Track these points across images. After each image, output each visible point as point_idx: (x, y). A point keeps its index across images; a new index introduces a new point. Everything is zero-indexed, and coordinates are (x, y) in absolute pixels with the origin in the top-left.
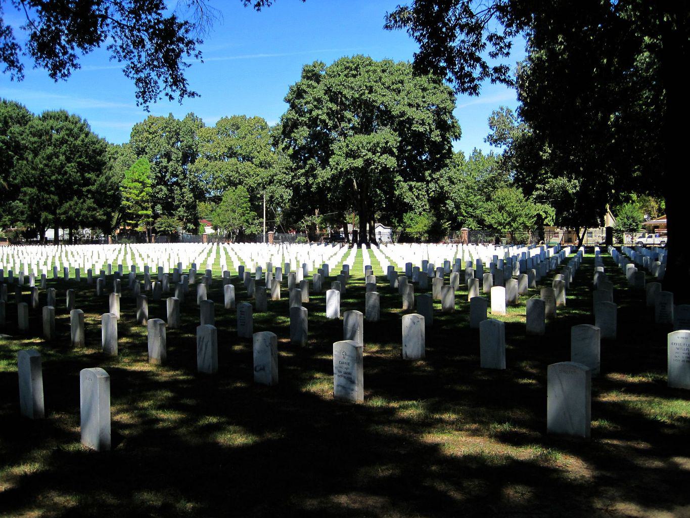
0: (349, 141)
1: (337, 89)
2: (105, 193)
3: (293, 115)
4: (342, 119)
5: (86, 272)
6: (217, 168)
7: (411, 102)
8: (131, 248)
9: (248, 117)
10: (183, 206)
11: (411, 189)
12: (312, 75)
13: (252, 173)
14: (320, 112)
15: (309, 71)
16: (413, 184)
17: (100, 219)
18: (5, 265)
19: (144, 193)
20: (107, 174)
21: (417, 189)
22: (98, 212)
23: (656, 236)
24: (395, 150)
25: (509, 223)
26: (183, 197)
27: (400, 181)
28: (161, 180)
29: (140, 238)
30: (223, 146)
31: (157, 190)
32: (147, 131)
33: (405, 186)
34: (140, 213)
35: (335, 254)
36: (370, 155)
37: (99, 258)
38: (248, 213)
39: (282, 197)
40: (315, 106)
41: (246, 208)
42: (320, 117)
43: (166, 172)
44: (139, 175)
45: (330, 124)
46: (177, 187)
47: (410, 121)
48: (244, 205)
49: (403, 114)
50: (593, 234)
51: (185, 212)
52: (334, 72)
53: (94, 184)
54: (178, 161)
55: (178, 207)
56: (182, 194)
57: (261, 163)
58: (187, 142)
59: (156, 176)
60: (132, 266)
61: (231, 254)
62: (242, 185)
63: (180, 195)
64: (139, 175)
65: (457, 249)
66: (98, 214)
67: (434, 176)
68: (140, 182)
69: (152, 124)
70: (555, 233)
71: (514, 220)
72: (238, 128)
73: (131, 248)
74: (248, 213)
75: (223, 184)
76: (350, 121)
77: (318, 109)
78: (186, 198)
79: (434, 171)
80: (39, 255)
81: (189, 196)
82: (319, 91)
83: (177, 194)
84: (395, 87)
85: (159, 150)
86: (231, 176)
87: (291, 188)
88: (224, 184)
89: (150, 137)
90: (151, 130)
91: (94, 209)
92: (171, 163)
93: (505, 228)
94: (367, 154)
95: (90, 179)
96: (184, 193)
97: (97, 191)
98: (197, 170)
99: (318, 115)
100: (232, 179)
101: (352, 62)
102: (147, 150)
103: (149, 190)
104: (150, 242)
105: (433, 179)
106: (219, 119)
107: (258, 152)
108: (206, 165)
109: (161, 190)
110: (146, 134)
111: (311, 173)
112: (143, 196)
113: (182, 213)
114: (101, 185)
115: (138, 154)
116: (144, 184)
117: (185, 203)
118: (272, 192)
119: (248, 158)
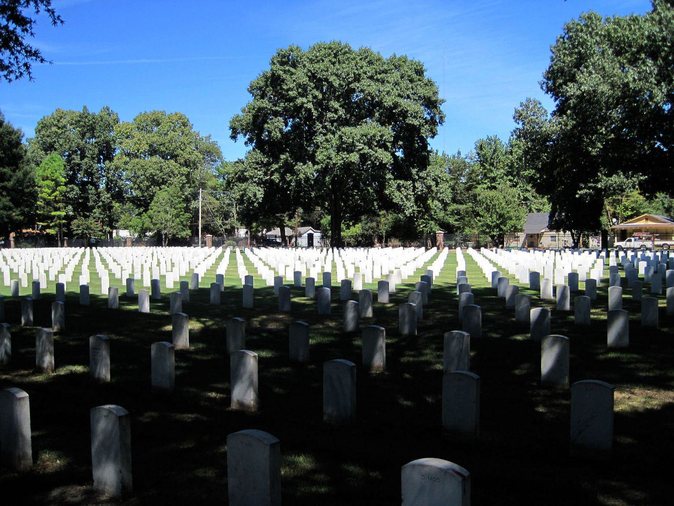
0: (342, 133)
1: (323, 75)
2: (22, 191)
3: (266, 104)
4: (328, 109)
5: (124, 283)
6: (139, 166)
7: (401, 93)
8: (99, 253)
9: (168, 113)
10: (99, 207)
11: (399, 188)
12: (287, 60)
13: (176, 172)
14: (304, 100)
15: (284, 56)
16: (402, 182)
17: (17, 220)
18: (163, 272)
19: (57, 193)
20: (25, 169)
21: (405, 188)
22: (14, 212)
23: (635, 240)
24: (389, 144)
25: (497, 226)
26: (99, 197)
27: (390, 179)
28: (71, 180)
29: (51, 242)
30: (144, 142)
31: (68, 190)
32: (56, 125)
33: (394, 184)
34: (53, 213)
35: (210, 256)
36: (366, 150)
37: (53, 263)
38: (183, 215)
39: (255, 195)
40: (299, 93)
41: (181, 208)
42: (305, 105)
43: (79, 170)
44: (52, 173)
45: (315, 114)
46: (91, 187)
47: (404, 114)
48: (179, 206)
49: (396, 105)
50: (557, 238)
51: (101, 214)
52: (317, 57)
53: (10, 181)
54: (93, 158)
55: (93, 208)
56: (98, 195)
57: (185, 162)
58: (105, 138)
59: (67, 175)
60: (246, 277)
61: (105, 256)
62: (165, 185)
63: (95, 195)
64: (52, 173)
65: (333, 255)
66: (14, 214)
67: (421, 174)
68: (52, 180)
69: (61, 118)
70: (515, 237)
71: (504, 223)
72: (158, 124)
73: (99, 253)
74: (183, 215)
75: (146, 183)
76: (336, 111)
77: (302, 96)
78: (102, 198)
79: (420, 170)
80: (149, 260)
81: (106, 196)
82: (301, 76)
83: (92, 194)
84: (379, 76)
85: (70, 146)
86: (155, 175)
87: (262, 186)
88: (148, 184)
89: (60, 131)
90: (60, 125)
91: (10, 209)
92: (86, 160)
93: (493, 231)
94: (363, 148)
95: (5, 173)
96: (100, 193)
97: (13, 189)
98: (117, 168)
99: (303, 103)
100: (156, 178)
101: (330, 48)
102: (57, 146)
103: (63, 188)
104: (62, 246)
105: (420, 177)
106: (137, 114)
107: (183, 150)
108: (126, 163)
109: (72, 190)
110: (54, 129)
111: (288, 168)
112: (56, 196)
113: (97, 214)
114: (18, 181)
115: (46, 150)
116: (57, 184)
117: (101, 204)
118: (245, 190)
119: (174, 157)
